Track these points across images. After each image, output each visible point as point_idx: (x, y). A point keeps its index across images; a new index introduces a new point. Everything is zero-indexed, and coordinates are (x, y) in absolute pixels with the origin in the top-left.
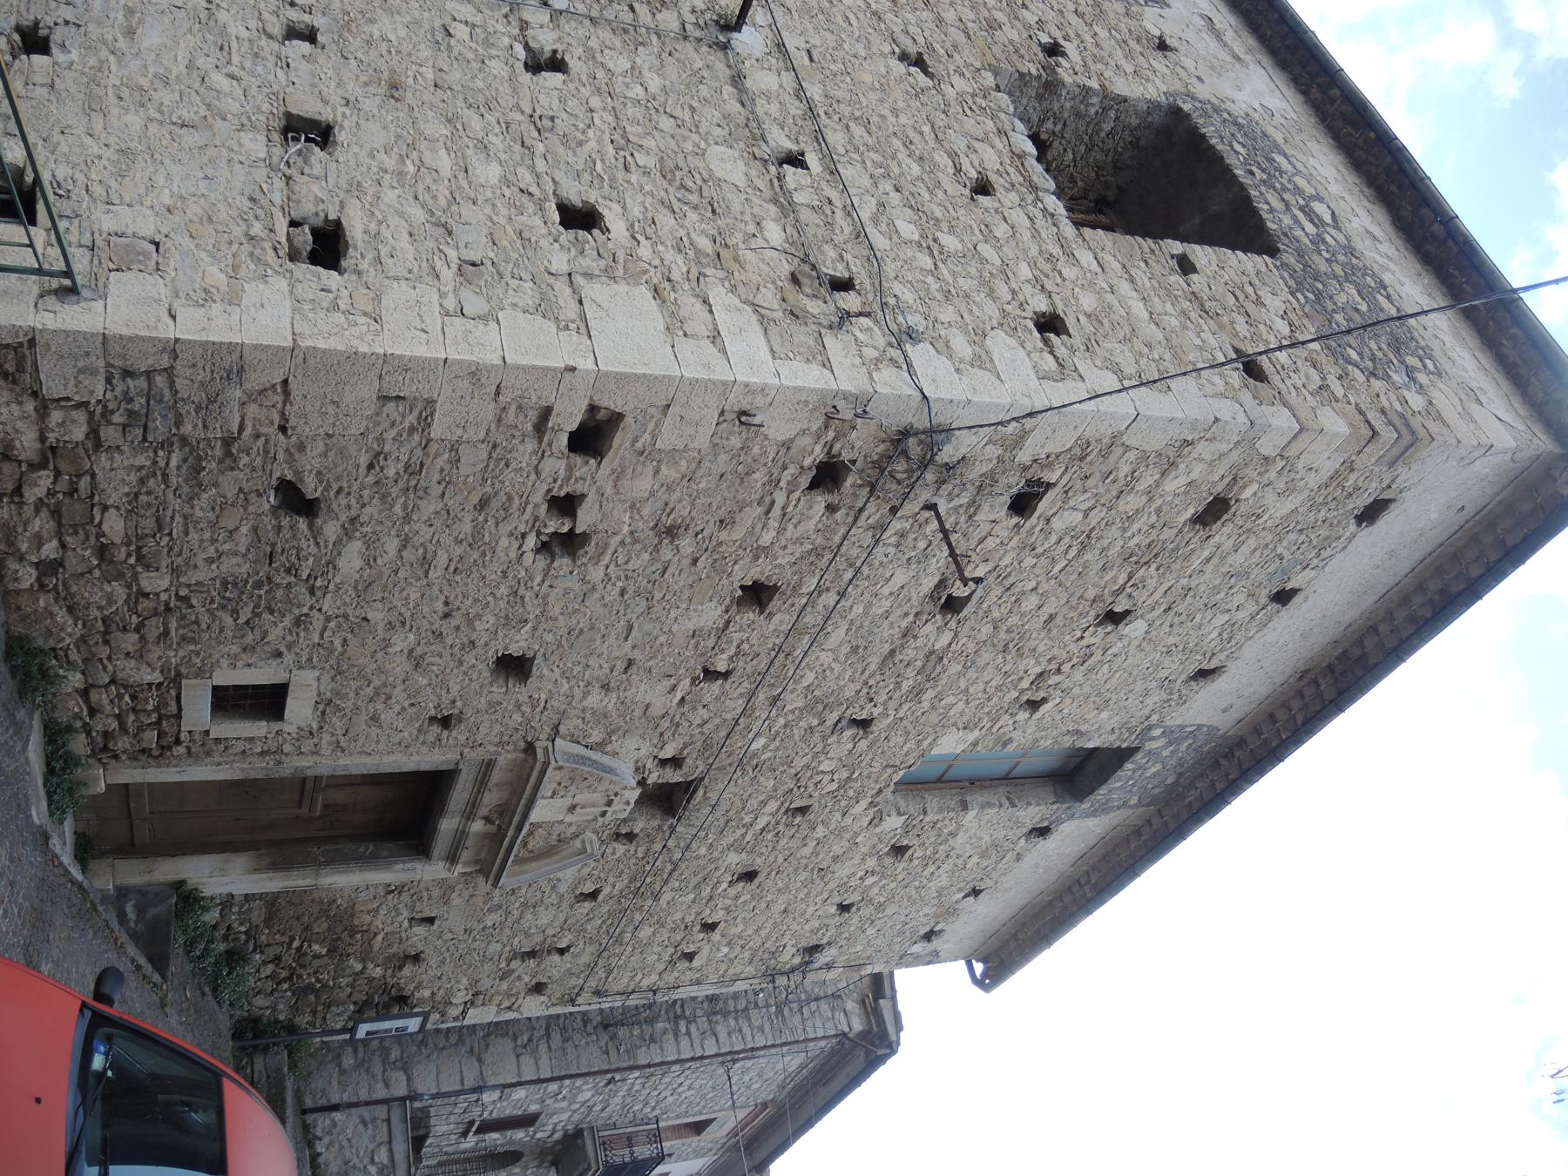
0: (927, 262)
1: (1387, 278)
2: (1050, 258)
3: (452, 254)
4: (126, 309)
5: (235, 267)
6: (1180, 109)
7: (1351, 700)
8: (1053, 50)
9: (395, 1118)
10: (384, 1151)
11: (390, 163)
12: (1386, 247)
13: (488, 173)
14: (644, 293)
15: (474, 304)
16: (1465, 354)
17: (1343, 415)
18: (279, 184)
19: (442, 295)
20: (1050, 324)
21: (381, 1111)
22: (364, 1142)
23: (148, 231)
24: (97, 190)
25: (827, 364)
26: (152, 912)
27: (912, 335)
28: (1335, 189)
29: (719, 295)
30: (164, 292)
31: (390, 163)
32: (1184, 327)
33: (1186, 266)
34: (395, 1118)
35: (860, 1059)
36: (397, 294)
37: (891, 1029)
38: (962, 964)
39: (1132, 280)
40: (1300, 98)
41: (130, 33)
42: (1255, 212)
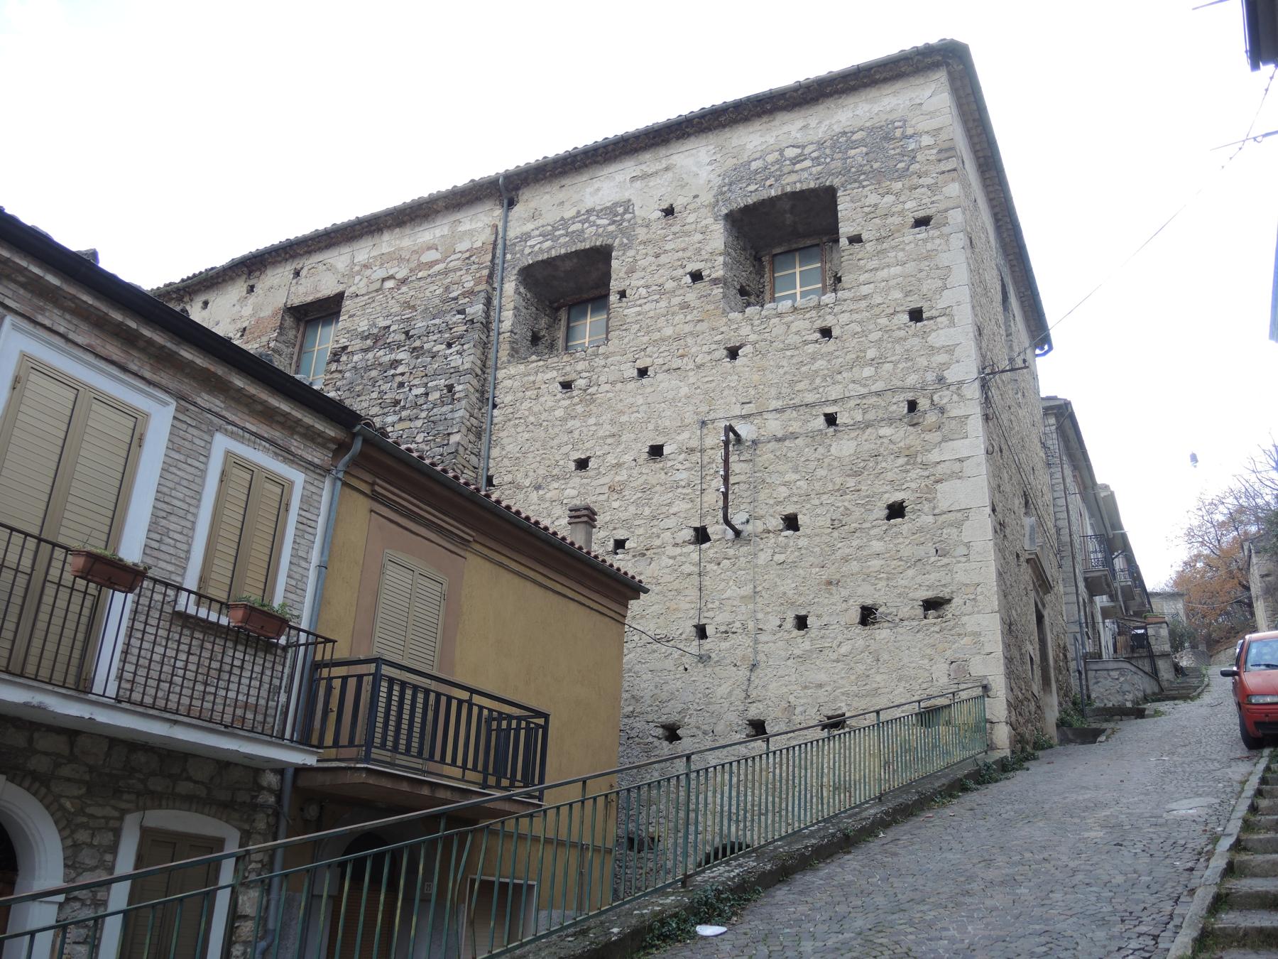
0: (888, 366)
1: (837, 129)
2: (870, 307)
3: (933, 559)
4: (992, 668)
5: (959, 635)
6: (727, 215)
7: (1001, 166)
8: (696, 277)
9: (1095, 667)
10: (1112, 673)
11: (883, 583)
12: (813, 122)
13: (877, 546)
14: (939, 486)
15: (962, 550)
16: (886, 101)
17: (946, 183)
18: (906, 623)
19: (959, 562)
20: (916, 315)
21: (1091, 674)
22: (1108, 683)
23: (947, 666)
24: (924, 686)
25: (967, 417)
26: (1070, 736)
27: (941, 379)
28: (770, 139)
29: (934, 456)
30: (978, 657)
31: (883, 583)
32: (903, 250)
33: (856, 240)
34: (1095, 667)
35: (1067, 423)
36: (961, 577)
37: (1057, 403)
38: (1038, 359)
39: (876, 269)
40: (692, 139)
41: (820, 686)
42: (802, 192)
